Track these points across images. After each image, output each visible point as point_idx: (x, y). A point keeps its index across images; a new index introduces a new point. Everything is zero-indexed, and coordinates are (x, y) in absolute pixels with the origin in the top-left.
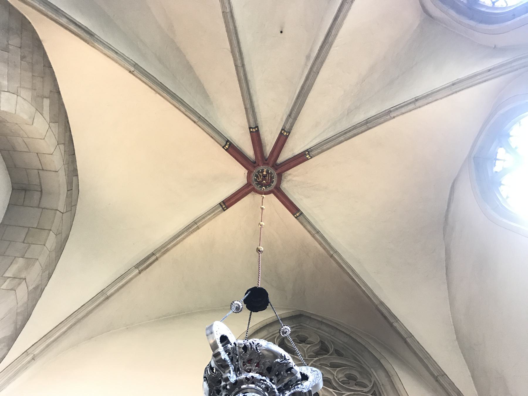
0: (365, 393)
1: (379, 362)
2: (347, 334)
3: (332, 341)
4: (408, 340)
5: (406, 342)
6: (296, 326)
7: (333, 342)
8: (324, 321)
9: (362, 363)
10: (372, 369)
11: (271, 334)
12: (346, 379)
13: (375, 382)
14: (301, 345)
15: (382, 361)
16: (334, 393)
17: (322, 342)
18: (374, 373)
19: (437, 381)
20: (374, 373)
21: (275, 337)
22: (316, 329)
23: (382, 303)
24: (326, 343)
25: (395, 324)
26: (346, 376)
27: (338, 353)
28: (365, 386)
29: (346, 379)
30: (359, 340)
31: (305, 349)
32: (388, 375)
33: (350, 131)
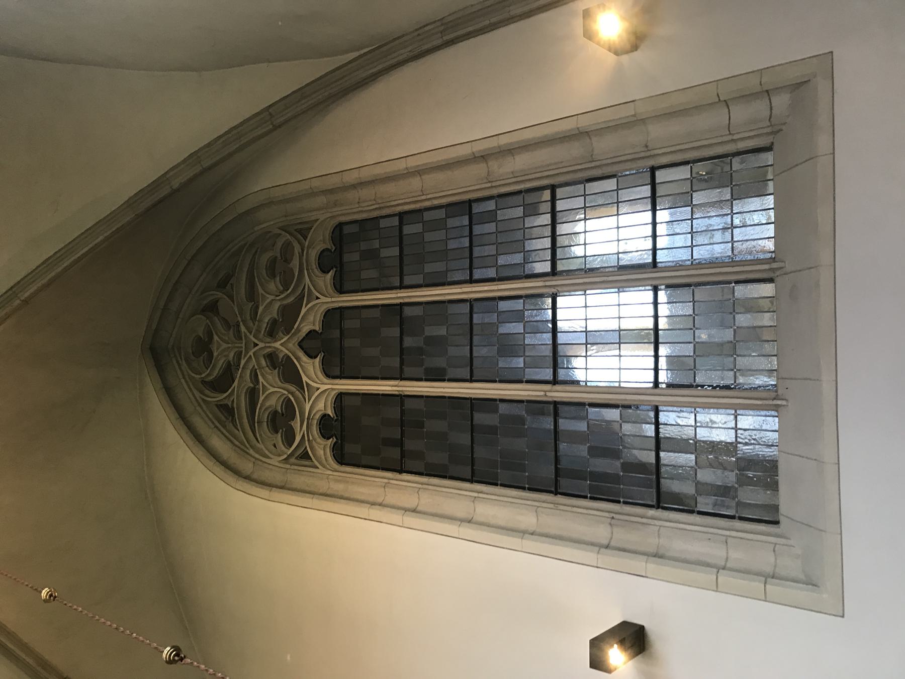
0: (303, 251)
1: (248, 212)
2: (188, 265)
3: (202, 293)
4: (207, 163)
5: (210, 168)
6: (175, 356)
7: (202, 293)
8: (162, 304)
9: (243, 243)
10: (256, 229)
11: (198, 408)
12: (278, 279)
13: (280, 228)
14: (215, 354)
15: (241, 209)
16: (309, 306)
17: (204, 311)
18: (263, 226)
19: (280, 126)
20: (263, 226)
21: (203, 400)
22: (179, 320)
23: (130, 203)
24: (205, 302)
25: (176, 184)
26: (273, 276)
27: (223, 285)
28: (287, 246)
29: (278, 279)
30: (200, 244)
31: (225, 346)
32: (270, 203)
33: (304, 112)
